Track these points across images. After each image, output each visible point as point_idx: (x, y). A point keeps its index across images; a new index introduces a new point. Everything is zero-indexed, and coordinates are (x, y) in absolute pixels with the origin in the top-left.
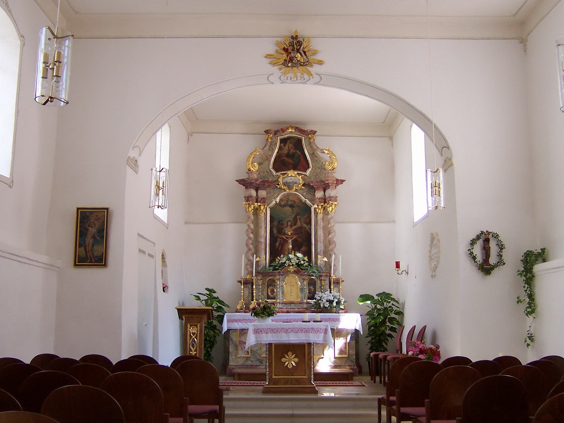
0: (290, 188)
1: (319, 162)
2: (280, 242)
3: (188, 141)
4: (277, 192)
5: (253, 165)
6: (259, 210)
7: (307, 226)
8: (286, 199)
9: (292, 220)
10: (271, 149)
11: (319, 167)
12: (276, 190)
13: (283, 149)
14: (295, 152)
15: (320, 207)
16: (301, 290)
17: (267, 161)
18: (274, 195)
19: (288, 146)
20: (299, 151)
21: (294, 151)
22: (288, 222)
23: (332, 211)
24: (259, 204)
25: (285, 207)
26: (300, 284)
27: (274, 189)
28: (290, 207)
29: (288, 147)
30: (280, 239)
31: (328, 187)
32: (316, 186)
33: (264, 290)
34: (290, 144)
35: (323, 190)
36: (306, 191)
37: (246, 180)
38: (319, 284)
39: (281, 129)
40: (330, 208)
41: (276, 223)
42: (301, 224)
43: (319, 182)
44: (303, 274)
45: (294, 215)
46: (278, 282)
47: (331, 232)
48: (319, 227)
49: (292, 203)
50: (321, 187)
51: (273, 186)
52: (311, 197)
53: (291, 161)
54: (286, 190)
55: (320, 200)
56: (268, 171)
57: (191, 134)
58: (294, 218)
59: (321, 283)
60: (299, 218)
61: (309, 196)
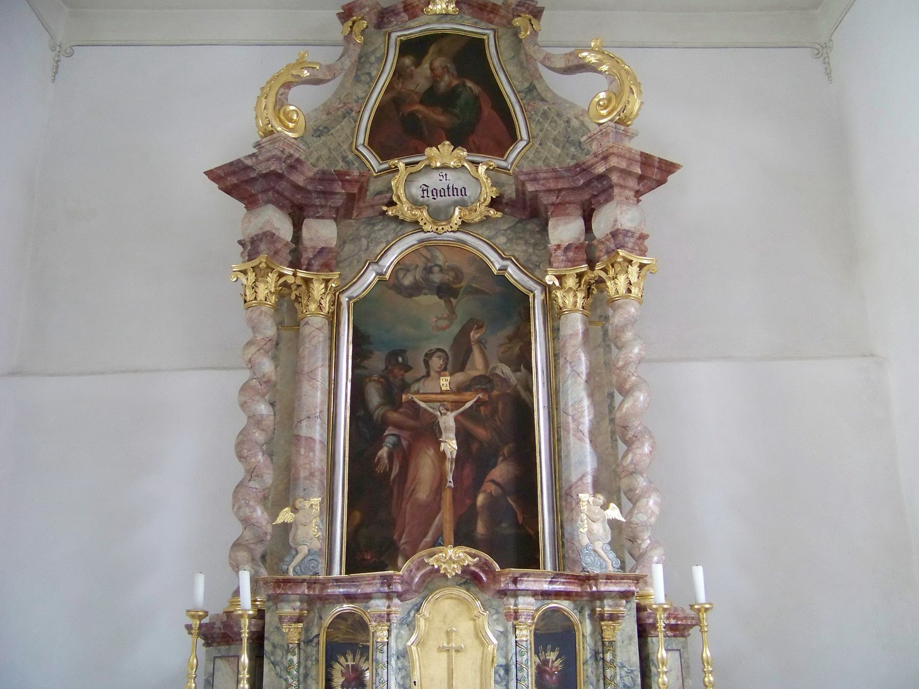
0: (439, 215)
1: (556, 118)
2: (397, 445)
3: (56, 73)
6: (304, 302)
8: (421, 263)
12: (380, 230)
13: (412, 76)
14: (457, 86)
15: (571, 282)
16: (502, 672)
17: (346, 120)
19: (431, 64)
20: (472, 80)
21: (455, 82)
22: (429, 355)
23: (629, 291)
24: (301, 274)
26: (495, 642)
30: (395, 432)
32: (553, 199)
33: (313, 673)
34: (439, 56)
35: (580, 212)
36: (505, 230)
37: (249, 162)
38: (589, 639)
41: (377, 362)
42: (584, 142)
43: (566, 174)
44: (512, 587)
45: (455, 329)
46: (382, 635)
48: (569, 371)
49: (449, 277)
50: (574, 203)
51: (369, 213)
52: (525, 251)
53: (442, 119)
55: (571, 254)
57: (68, 51)
58: (456, 340)
59: (598, 632)
60: (479, 342)
61: (520, 250)
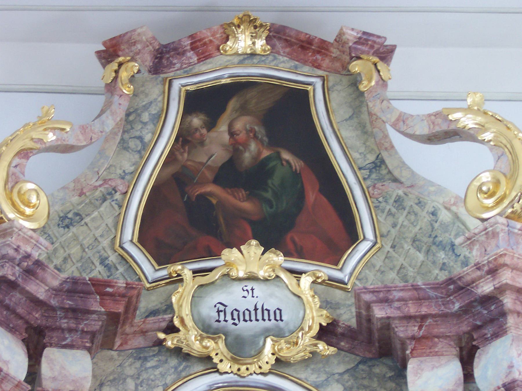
1: (416, 208)
4: (163, 375)
5: (15, 191)
10: (133, 144)
11: (414, 240)
12: (155, 367)
13: (202, 143)
21: (266, 153)
27: (145, 359)
29: (232, 134)
31: (489, 331)
32: (413, 330)
35: (455, 351)
36: (341, 374)
39: (192, 37)
51: (139, 342)
53: (247, 205)
54: (216, 360)
56: (113, 258)
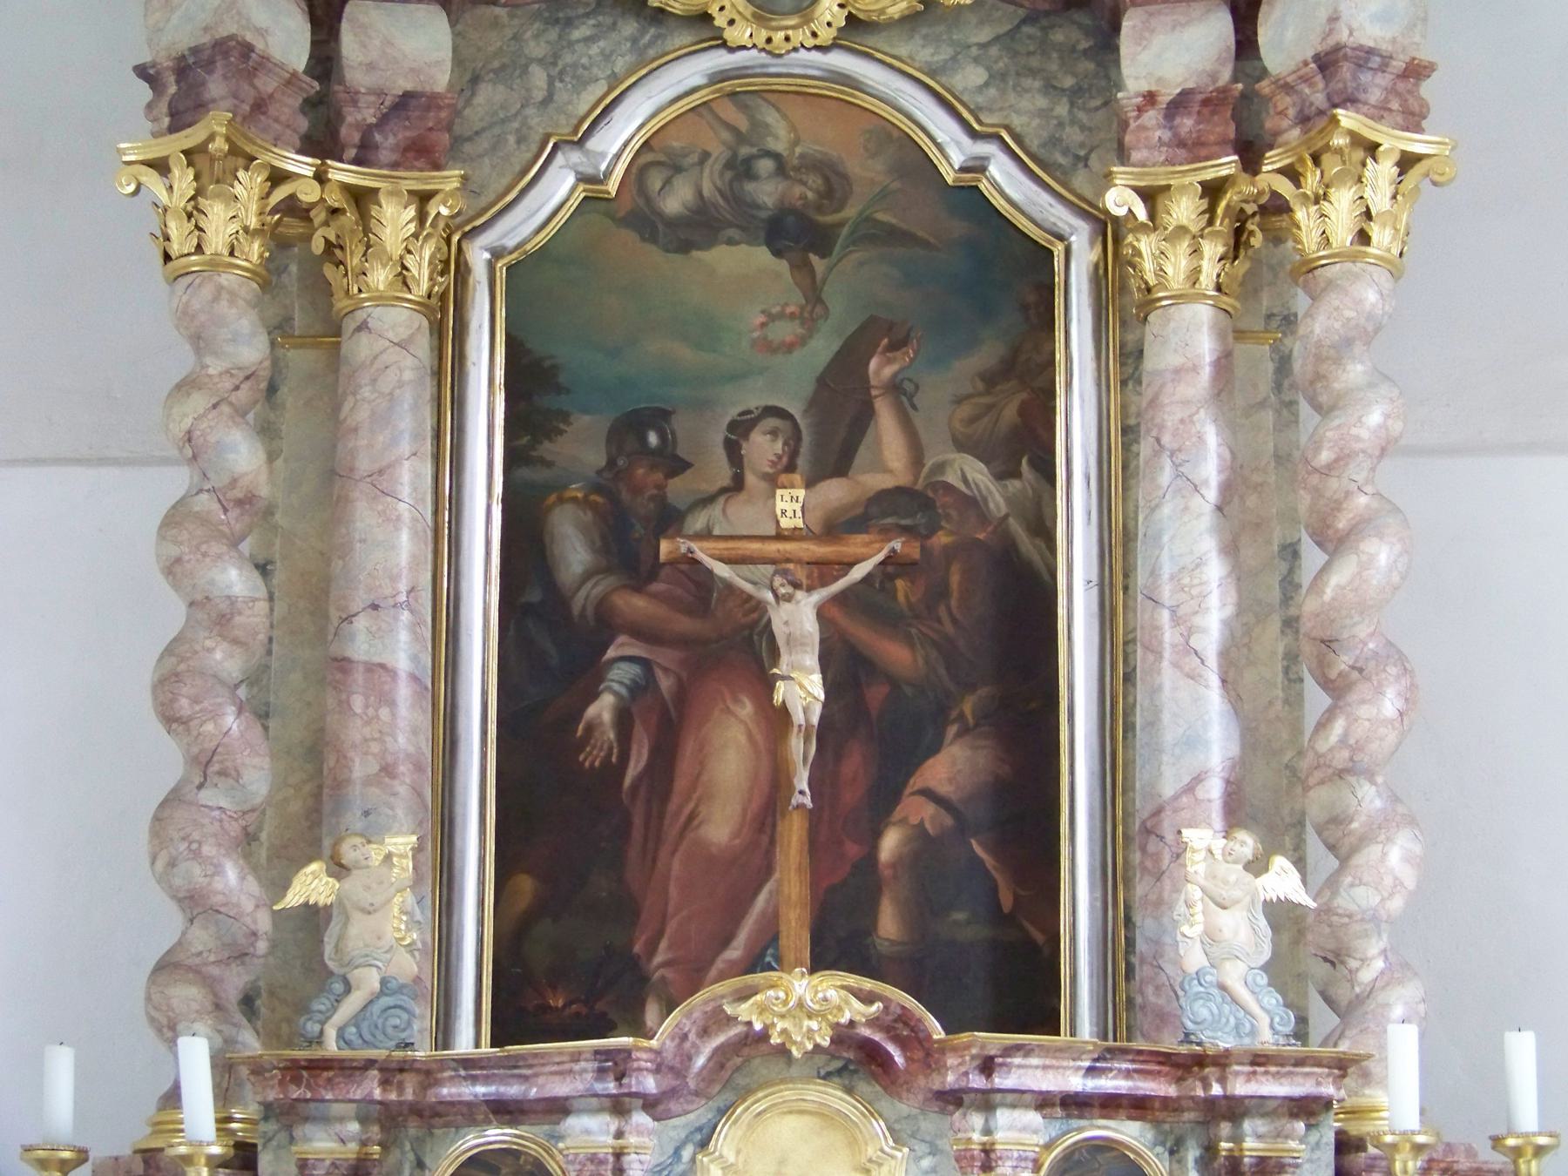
2: (642, 688)
6: (354, 261)
7: (1000, 476)
8: (716, 145)
9: (795, 410)
12: (589, 40)
15: (1184, 209)
18: (562, 96)
22: (741, 428)
23: (1363, 237)
25: (709, 244)
28: (769, 244)
40: (1342, 208)
44: (977, 1081)
45: (822, 349)
47: (1342, 524)
49: (805, 191)
52: (1044, 114)
55: (1187, 124)
60: (895, 388)
